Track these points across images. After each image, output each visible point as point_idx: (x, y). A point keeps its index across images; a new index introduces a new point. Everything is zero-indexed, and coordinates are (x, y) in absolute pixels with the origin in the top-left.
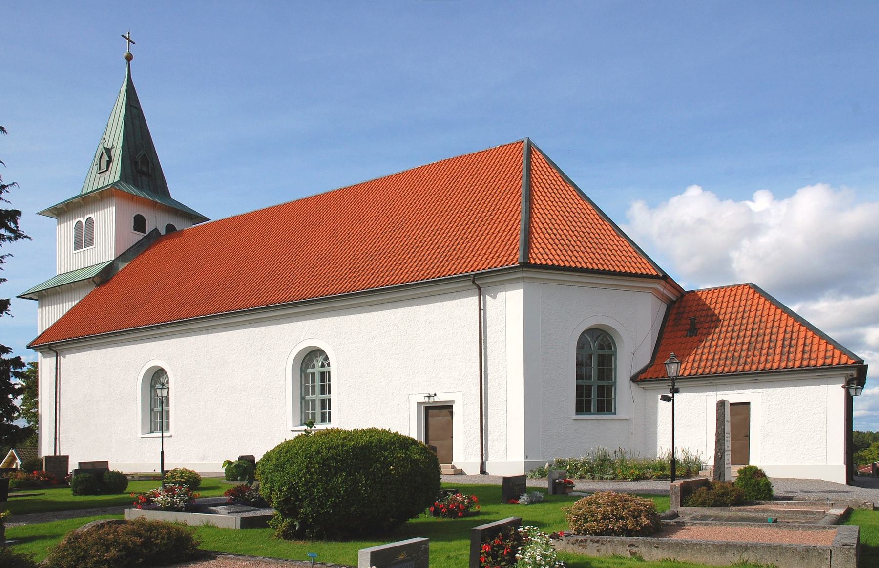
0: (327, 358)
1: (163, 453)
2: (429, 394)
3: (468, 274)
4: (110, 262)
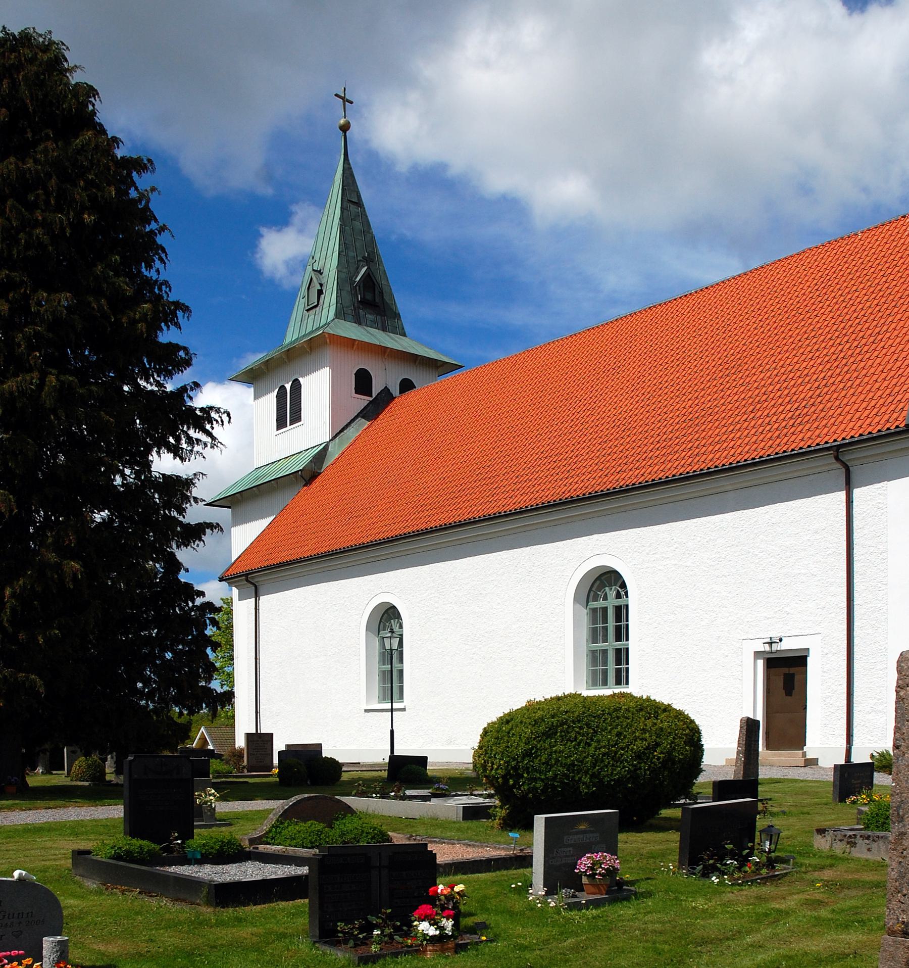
0: (623, 585)
1: (392, 732)
2: (771, 638)
3: (828, 445)
4: (324, 445)
